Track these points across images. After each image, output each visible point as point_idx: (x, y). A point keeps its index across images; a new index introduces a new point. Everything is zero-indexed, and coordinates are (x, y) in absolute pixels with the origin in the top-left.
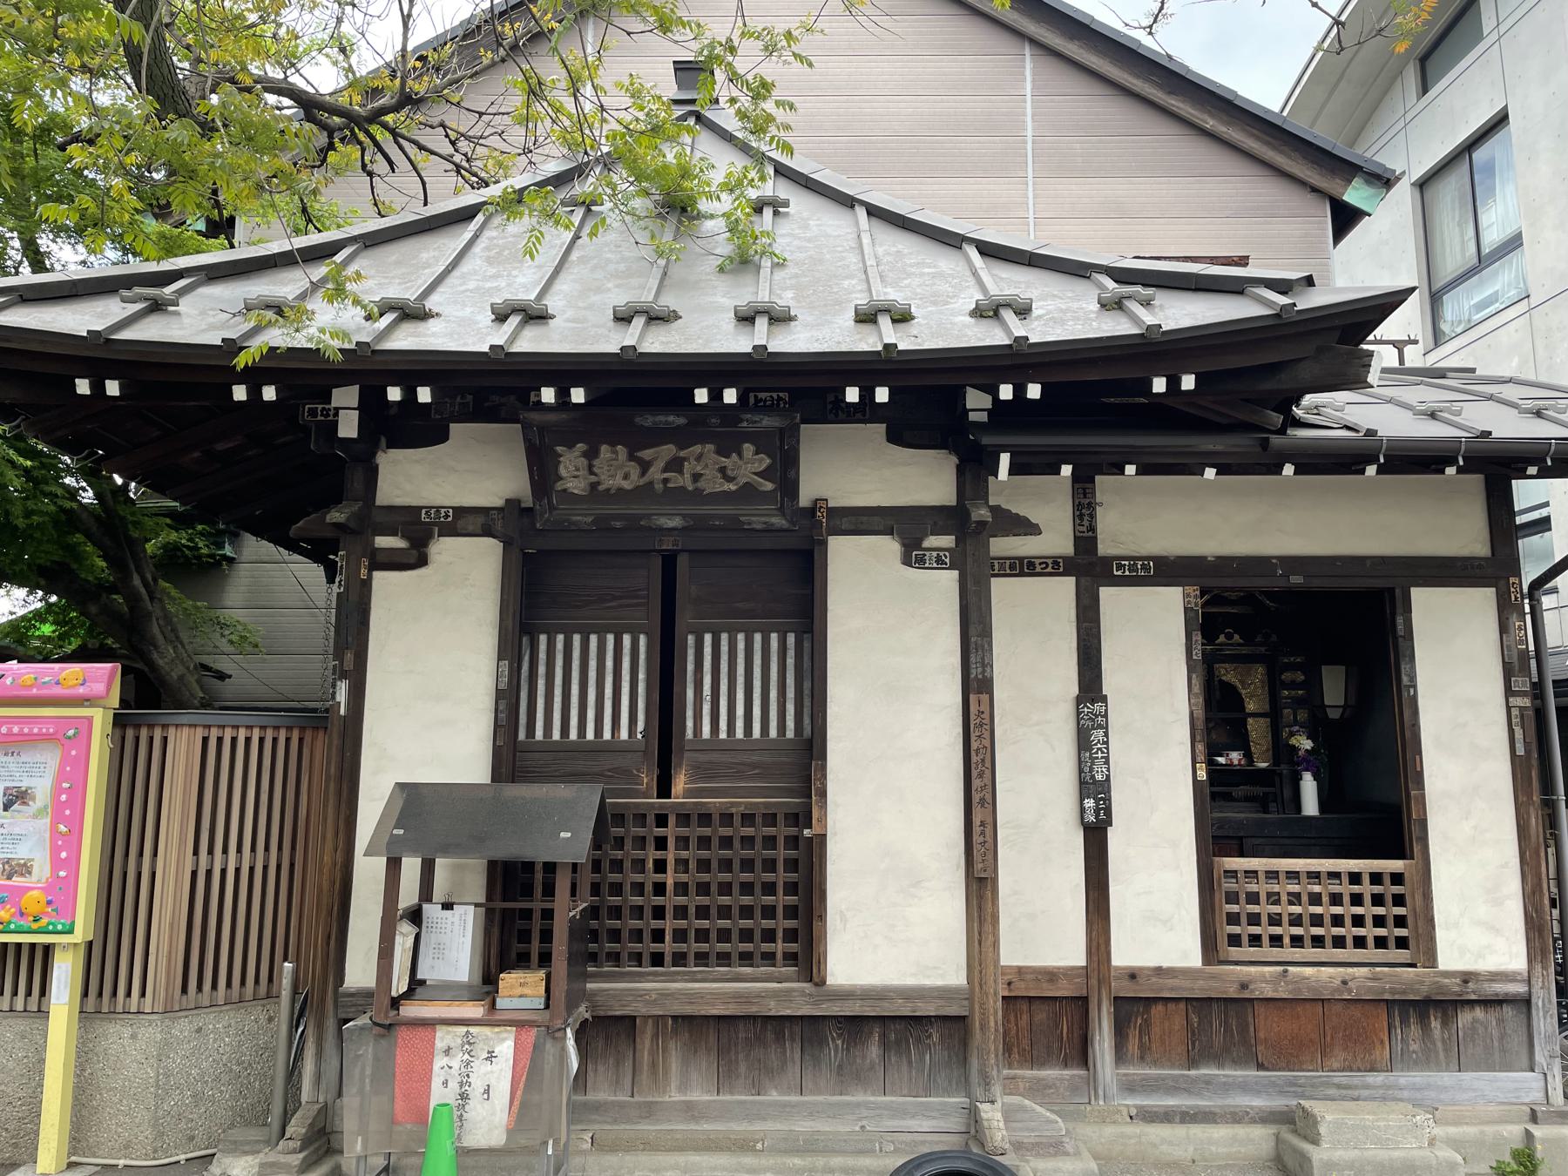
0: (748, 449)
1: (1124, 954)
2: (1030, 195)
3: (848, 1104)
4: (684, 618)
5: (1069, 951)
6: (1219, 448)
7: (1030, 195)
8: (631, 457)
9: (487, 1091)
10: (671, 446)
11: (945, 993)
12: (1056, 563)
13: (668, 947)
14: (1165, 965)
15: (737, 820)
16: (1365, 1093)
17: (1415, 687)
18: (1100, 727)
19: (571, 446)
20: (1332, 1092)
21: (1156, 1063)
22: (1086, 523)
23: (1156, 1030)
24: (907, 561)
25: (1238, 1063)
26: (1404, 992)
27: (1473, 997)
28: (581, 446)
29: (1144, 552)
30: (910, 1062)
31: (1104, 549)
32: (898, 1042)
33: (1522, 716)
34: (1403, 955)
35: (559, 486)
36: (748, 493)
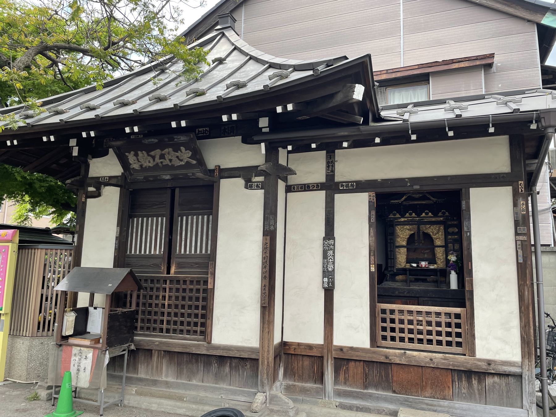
0: (183, 148)
1: (339, 340)
2: (402, 42)
3: (217, 388)
4: (177, 211)
5: (318, 339)
6: (346, 133)
7: (402, 42)
9: (85, 369)
10: (159, 150)
11: (252, 350)
12: (318, 186)
13: (165, 326)
14: (355, 345)
15: (188, 282)
16: (440, 409)
17: (470, 232)
18: (331, 249)
19: (130, 153)
20: (424, 406)
21: (350, 386)
22: (330, 169)
23: (351, 373)
24: (246, 187)
25: (384, 389)
26: (459, 367)
27: (493, 372)
29: (353, 179)
30: (239, 375)
31: (337, 179)
32: (235, 367)
33: (522, 245)
34: (459, 350)
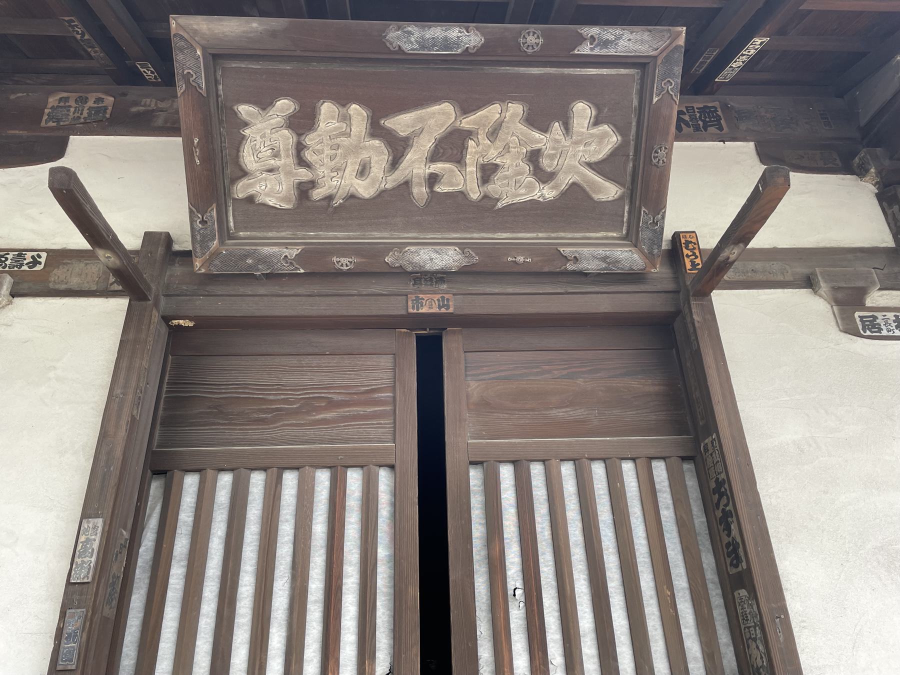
0: (582, 111)
8: (376, 130)
19: (264, 103)
24: (851, 330)
28: (285, 106)
35: (241, 190)
36: (574, 206)
